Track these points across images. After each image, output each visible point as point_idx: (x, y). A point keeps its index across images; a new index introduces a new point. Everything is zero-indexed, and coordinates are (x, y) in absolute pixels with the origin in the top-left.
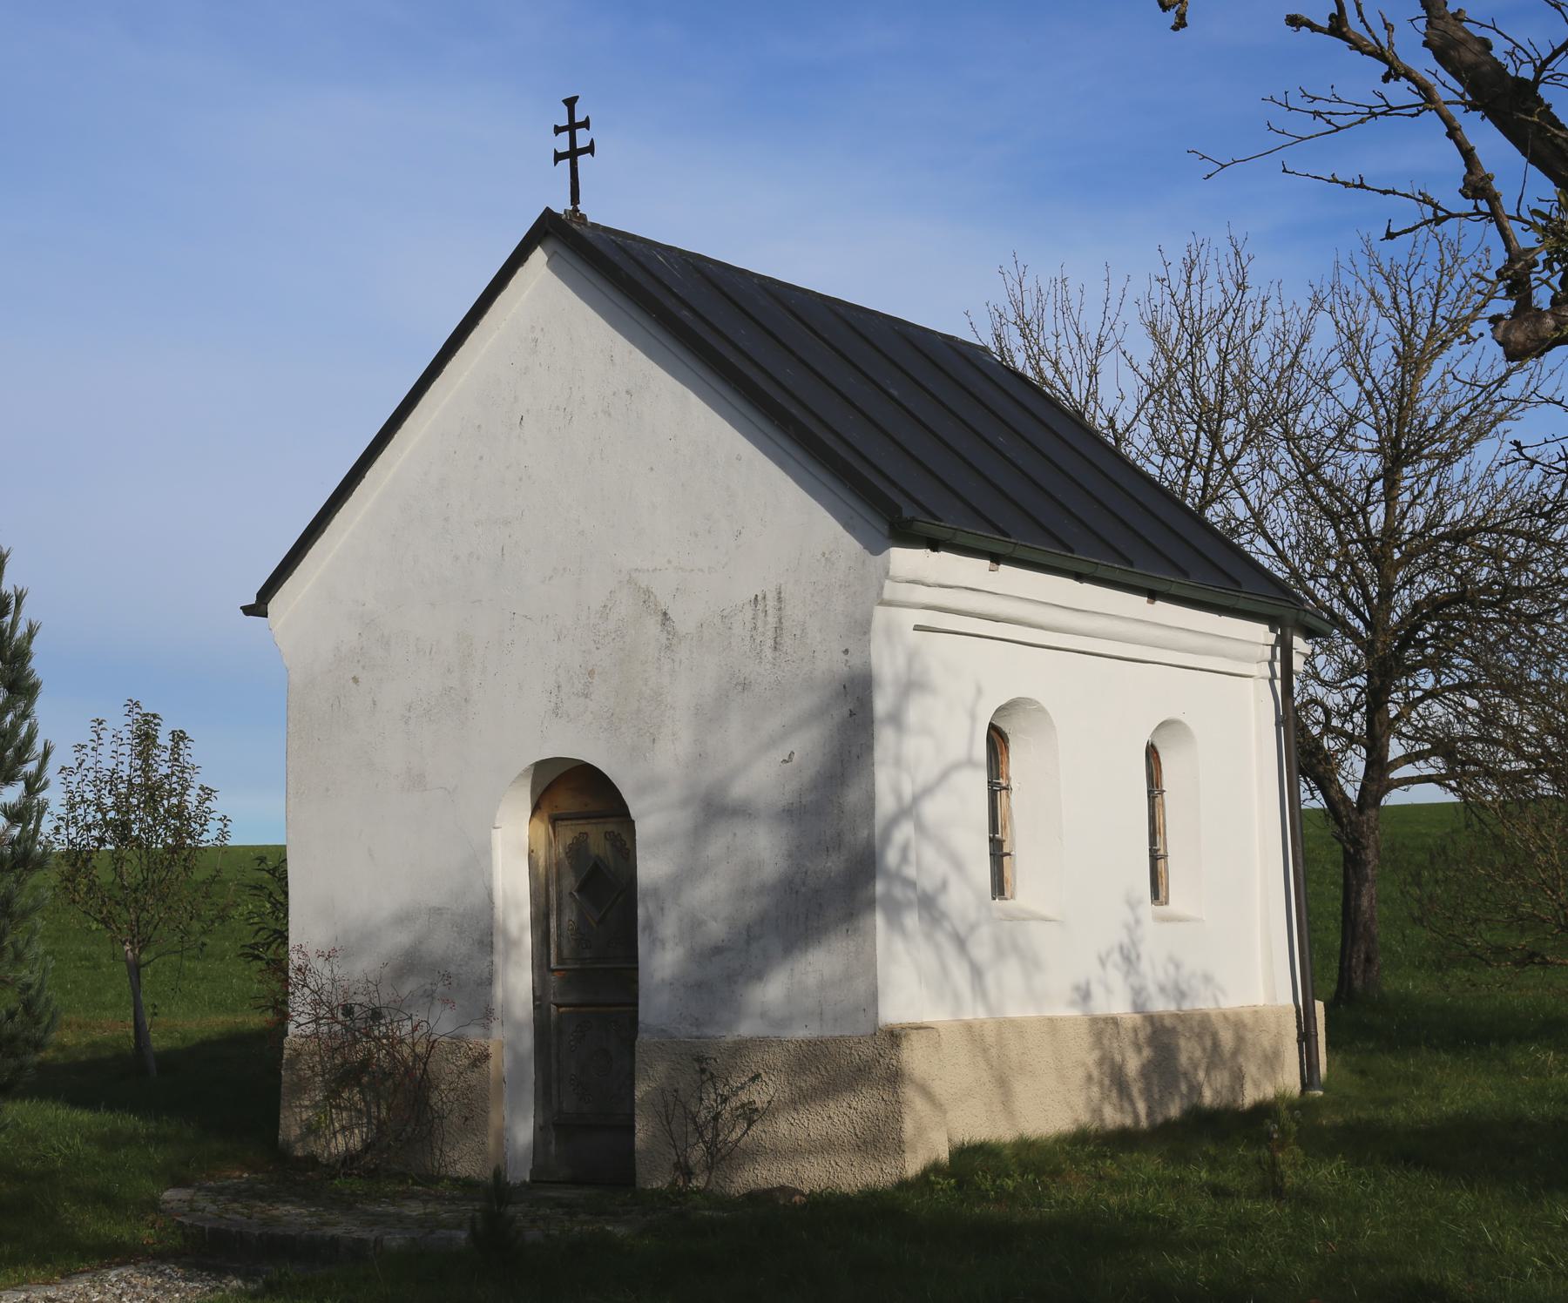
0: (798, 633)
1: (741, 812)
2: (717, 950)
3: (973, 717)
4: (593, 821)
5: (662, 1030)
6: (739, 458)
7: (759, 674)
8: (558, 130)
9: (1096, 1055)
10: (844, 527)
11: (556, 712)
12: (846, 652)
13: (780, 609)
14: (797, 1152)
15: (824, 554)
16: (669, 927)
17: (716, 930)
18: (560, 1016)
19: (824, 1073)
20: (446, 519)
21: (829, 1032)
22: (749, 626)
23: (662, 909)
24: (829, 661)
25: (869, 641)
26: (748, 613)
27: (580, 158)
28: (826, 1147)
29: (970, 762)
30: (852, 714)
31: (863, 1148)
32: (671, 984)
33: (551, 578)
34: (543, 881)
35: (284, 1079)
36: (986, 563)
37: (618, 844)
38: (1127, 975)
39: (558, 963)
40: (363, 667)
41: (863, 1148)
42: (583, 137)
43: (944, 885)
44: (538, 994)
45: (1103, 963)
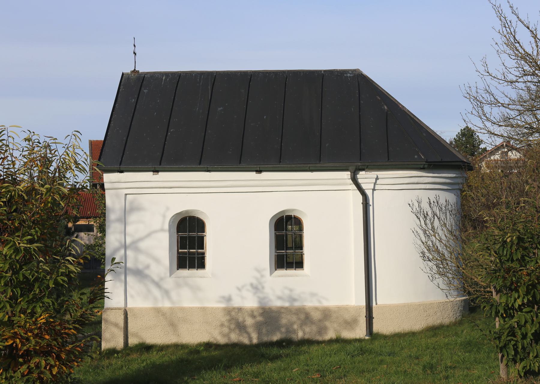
3: (164, 216)
9: (228, 318)
29: (162, 230)
36: (152, 173)
38: (255, 294)
43: (148, 267)
45: (239, 289)
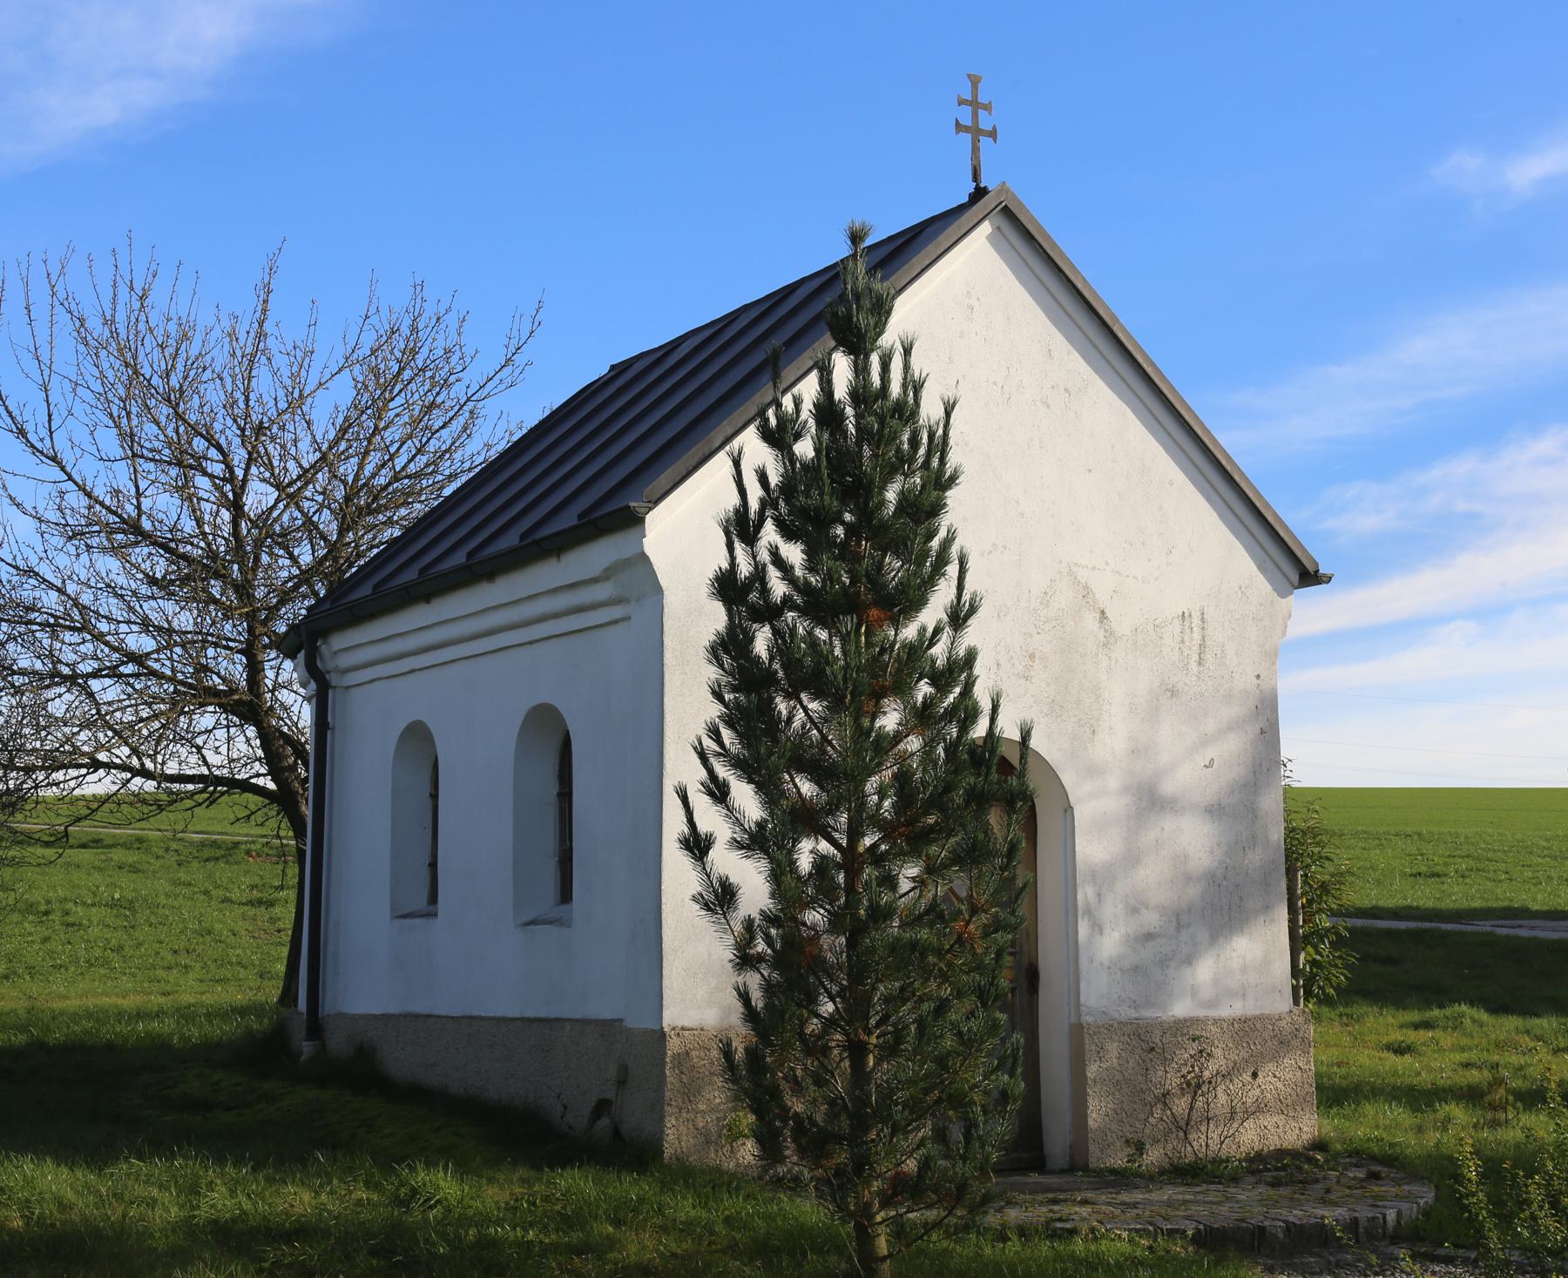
0: (1218, 652)
2: (1149, 937)
5: (1104, 1013)
12: (1258, 677)
15: (1240, 588)
16: (1111, 909)
17: (1151, 920)
22: (1178, 639)
23: (1099, 895)
30: (1262, 732)
33: (990, 552)
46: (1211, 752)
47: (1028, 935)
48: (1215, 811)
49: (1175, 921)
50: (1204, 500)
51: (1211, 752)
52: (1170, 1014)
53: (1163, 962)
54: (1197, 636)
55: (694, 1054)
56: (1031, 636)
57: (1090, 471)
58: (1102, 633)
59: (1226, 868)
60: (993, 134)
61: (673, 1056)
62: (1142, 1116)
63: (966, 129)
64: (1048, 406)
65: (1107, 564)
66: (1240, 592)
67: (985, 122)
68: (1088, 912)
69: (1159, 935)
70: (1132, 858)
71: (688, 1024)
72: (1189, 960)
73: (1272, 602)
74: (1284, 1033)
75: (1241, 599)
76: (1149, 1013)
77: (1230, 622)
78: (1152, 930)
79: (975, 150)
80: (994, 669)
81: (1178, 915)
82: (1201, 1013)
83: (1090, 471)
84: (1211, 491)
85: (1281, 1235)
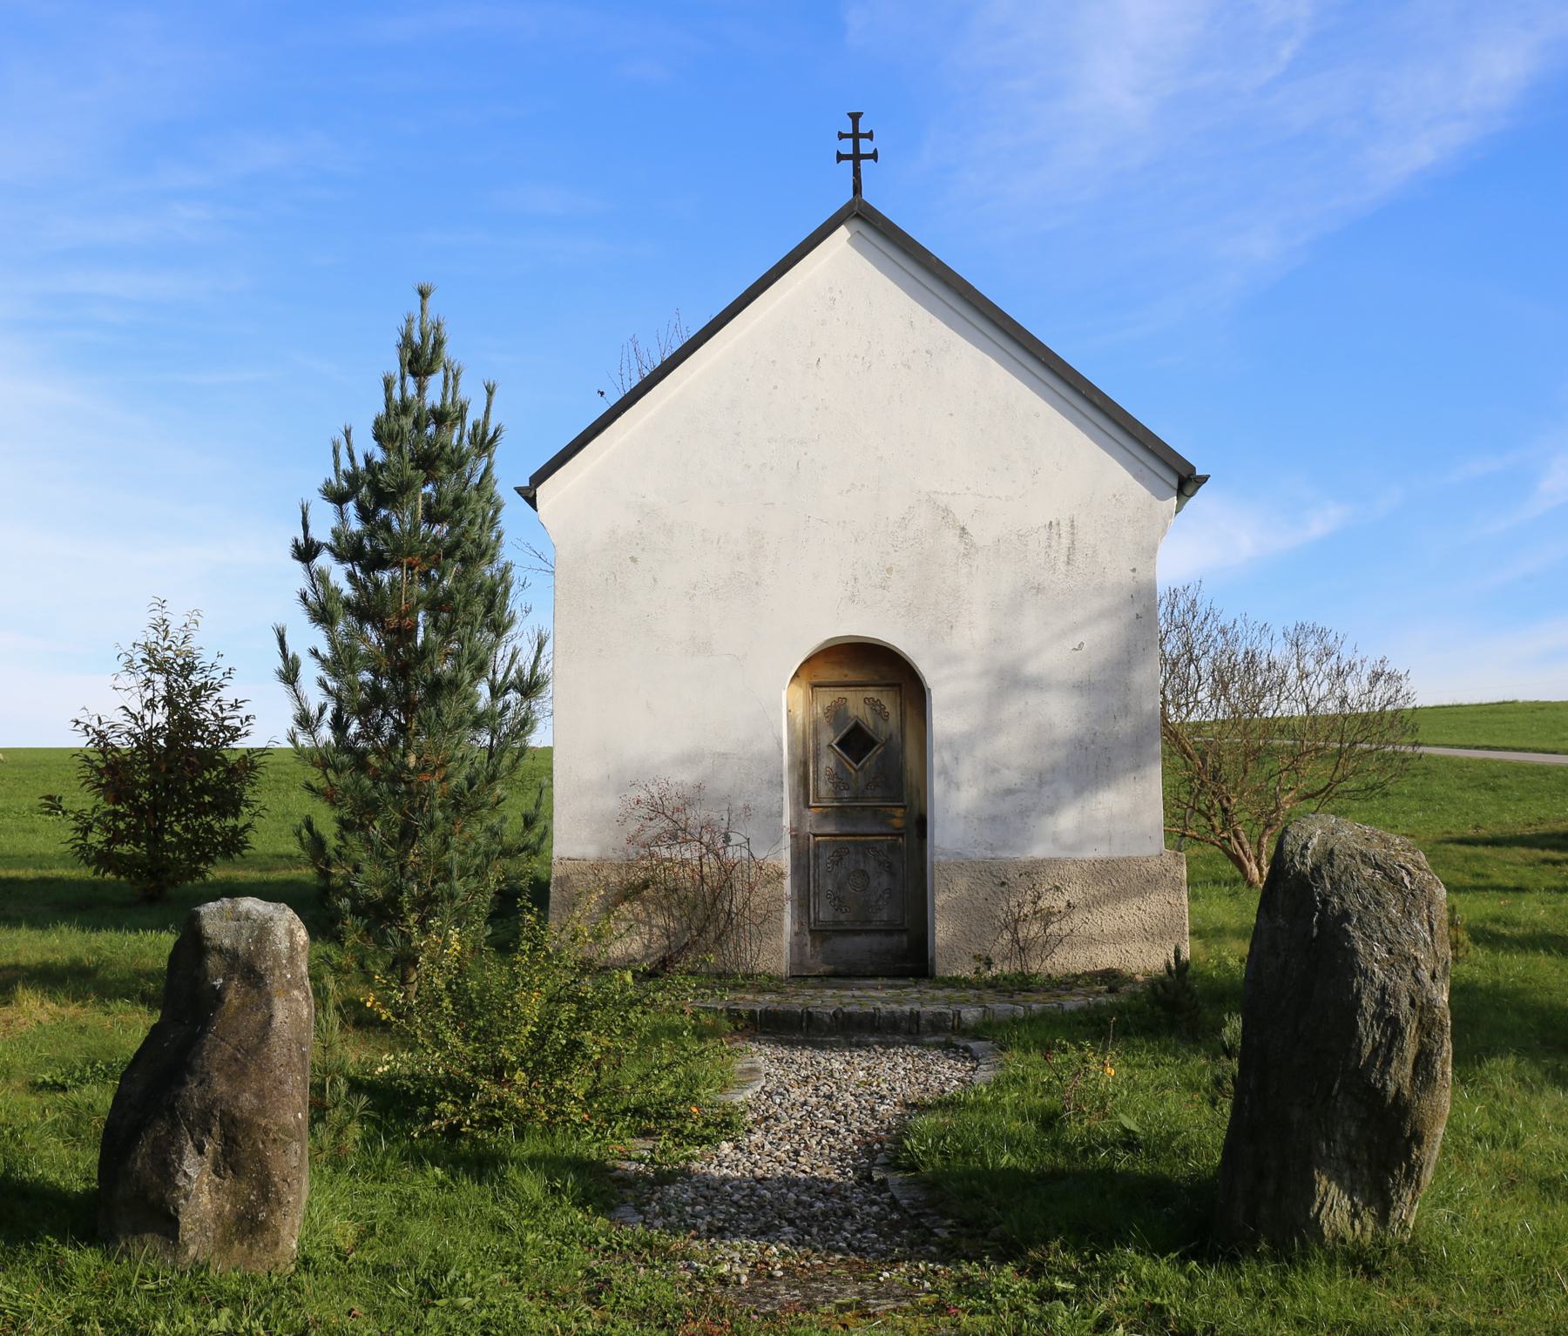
0: (1090, 553)
1: (1035, 684)
2: (1009, 792)
4: (852, 689)
5: (958, 853)
6: (1037, 415)
7: (1052, 581)
8: (841, 136)
10: (1134, 477)
11: (852, 598)
12: (1134, 570)
13: (1073, 534)
14: (1091, 940)
15: (1115, 496)
16: (965, 771)
17: (1011, 778)
18: (817, 845)
19: (1115, 884)
20: (738, 434)
21: (1117, 852)
22: (1044, 544)
23: (957, 759)
24: (1118, 571)
25: (1155, 564)
26: (1044, 534)
27: (863, 162)
28: (1120, 937)
30: (1138, 617)
31: (1151, 939)
32: (965, 817)
33: (848, 491)
34: (801, 734)
35: (552, 895)
37: (878, 708)
39: (814, 802)
40: (643, 550)
41: (1151, 939)
42: (866, 147)
44: (794, 826)
46: (1081, 637)
47: (918, 792)
48: (1083, 687)
49: (1036, 779)
50: (1074, 426)
51: (1081, 637)
52: (1029, 855)
53: (1024, 813)
54: (1065, 541)
55: (574, 877)
56: (888, 553)
57: (951, 415)
58: (963, 545)
59: (1095, 734)
60: (874, 156)
61: (557, 878)
62: (991, 938)
63: (847, 157)
64: (909, 367)
65: (968, 489)
66: (1114, 501)
67: (866, 147)
68: (945, 772)
69: (1020, 791)
70: (990, 729)
71: (572, 855)
72: (1051, 811)
73: (1151, 505)
74: (1151, 872)
75: (1115, 505)
76: (1006, 854)
77: (1103, 526)
78: (1013, 786)
79: (857, 172)
80: (853, 582)
81: (1041, 774)
82: (1062, 855)
83: (951, 415)
84: (1078, 416)
85: (828, 1020)
